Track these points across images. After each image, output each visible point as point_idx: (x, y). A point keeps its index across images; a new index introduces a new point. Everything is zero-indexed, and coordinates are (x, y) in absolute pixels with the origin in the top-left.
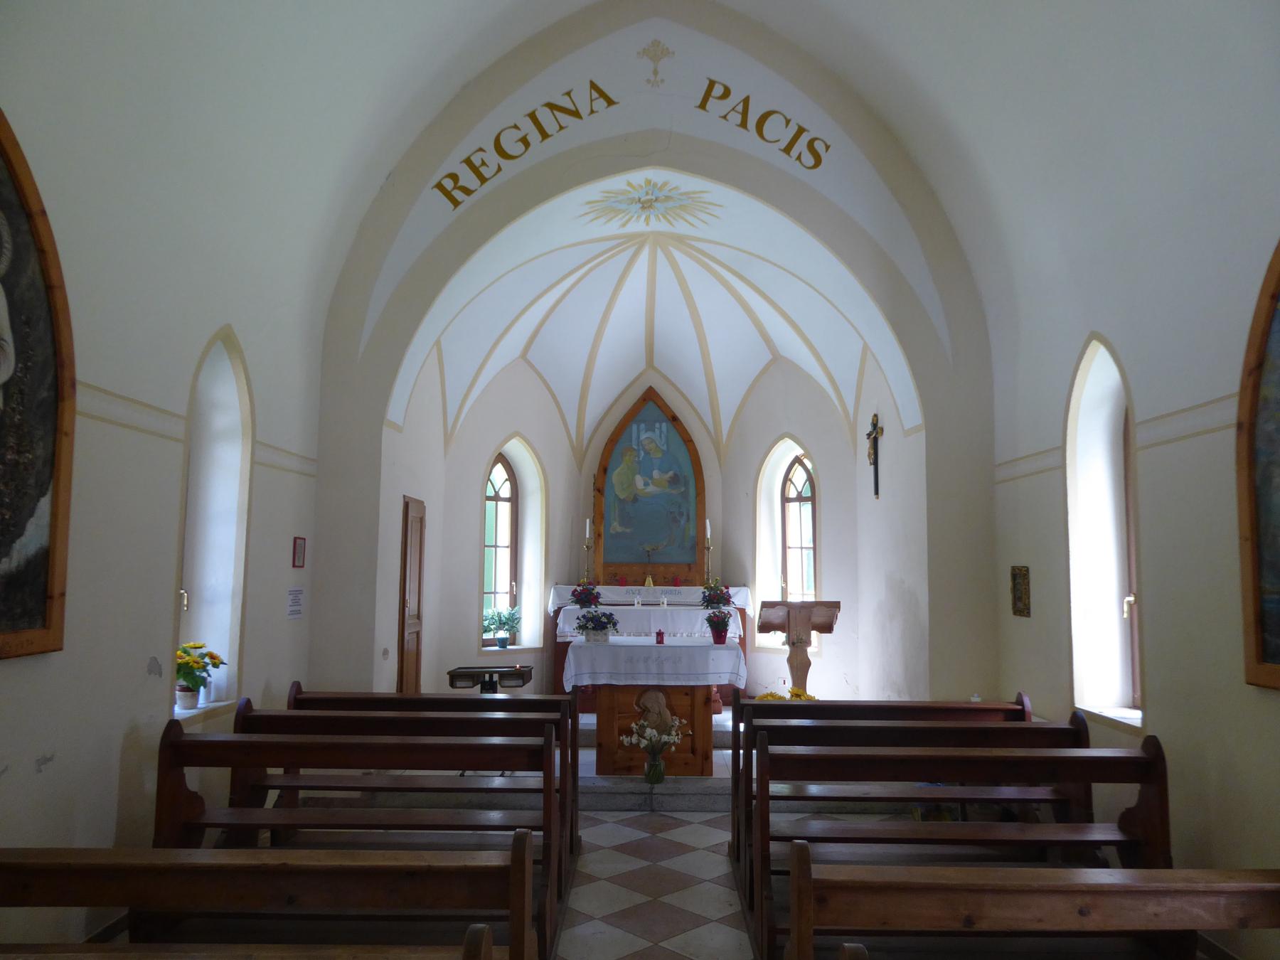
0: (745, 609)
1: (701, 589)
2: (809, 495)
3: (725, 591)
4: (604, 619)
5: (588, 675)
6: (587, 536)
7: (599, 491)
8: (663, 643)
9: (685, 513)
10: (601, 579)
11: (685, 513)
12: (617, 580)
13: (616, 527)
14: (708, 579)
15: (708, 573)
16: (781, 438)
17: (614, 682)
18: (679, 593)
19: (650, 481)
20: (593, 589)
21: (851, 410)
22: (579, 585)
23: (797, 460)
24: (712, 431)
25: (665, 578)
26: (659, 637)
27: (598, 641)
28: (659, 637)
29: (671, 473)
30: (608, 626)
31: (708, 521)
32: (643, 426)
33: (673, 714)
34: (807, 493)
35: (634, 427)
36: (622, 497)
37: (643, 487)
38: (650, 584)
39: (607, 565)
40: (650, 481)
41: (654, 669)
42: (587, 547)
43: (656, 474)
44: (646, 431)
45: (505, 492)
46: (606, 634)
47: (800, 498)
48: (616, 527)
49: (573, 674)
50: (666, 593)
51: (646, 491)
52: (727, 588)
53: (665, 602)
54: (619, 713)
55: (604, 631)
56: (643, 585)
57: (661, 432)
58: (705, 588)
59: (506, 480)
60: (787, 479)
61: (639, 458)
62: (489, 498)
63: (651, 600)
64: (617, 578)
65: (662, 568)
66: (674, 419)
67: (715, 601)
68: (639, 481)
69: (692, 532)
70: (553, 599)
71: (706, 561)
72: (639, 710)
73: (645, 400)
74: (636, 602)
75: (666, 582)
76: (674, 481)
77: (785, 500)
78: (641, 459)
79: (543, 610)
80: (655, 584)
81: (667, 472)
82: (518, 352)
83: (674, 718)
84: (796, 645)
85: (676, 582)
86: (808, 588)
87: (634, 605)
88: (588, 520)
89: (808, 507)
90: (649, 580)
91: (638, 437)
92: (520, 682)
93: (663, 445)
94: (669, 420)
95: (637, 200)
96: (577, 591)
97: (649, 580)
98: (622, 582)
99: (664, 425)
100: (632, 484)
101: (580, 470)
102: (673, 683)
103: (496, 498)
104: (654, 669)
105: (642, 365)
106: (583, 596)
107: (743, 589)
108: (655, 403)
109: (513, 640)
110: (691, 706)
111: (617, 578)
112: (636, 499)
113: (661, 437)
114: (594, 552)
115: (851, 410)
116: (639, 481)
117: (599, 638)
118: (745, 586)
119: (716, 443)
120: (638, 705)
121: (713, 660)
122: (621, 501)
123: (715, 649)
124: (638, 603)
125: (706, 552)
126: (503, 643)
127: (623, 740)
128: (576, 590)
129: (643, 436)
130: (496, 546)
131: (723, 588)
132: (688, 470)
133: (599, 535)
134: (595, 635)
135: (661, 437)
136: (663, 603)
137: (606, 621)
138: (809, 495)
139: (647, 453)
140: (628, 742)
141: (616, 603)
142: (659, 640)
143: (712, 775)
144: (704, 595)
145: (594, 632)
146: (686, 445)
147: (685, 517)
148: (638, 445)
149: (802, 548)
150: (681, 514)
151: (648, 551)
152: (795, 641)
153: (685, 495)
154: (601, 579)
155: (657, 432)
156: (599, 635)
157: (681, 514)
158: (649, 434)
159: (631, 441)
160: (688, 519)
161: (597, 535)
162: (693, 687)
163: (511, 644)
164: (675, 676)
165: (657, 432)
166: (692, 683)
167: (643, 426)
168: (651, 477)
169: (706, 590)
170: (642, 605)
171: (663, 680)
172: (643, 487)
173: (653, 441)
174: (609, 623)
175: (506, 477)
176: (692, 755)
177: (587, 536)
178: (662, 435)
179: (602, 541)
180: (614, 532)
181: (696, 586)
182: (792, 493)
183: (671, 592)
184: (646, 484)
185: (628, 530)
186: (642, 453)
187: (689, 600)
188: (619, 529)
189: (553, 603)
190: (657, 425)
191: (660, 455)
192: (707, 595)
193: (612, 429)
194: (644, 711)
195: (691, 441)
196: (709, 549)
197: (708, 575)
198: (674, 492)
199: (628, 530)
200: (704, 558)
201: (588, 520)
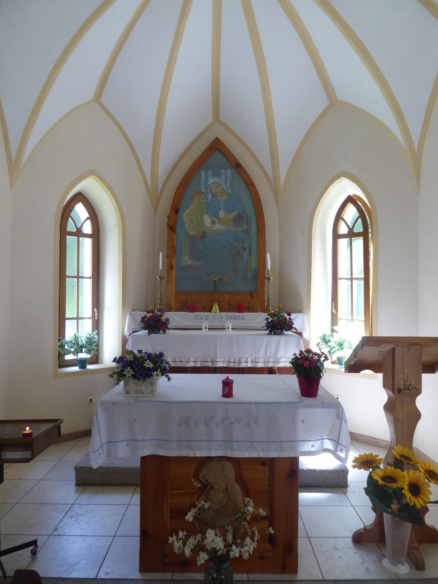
0: (302, 333)
1: (264, 315)
2: (361, 230)
3: (288, 317)
4: (148, 364)
5: (125, 443)
6: (161, 268)
7: (172, 228)
8: (232, 396)
9: (247, 248)
10: (173, 305)
11: (247, 248)
12: (187, 307)
13: (187, 260)
14: (268, 306)
15: (268, 300)
16: (337, 177)
17: (162, 453)
18: (243, 318)
19: (217, 220)
20: (161, 316)
21: (416, 139)
22: (148, 312)
23: (350, 200)
24: (271, 178)
25: (230, 305)
26: (227, 388)
27: (141, 392)
28: (227, 388)
29: (235, 214)
30: (154, 373)
31: (268, 255)
32: (210, 172)
33: (247, 493)
34: (359, 228)
35: (203, 173)
36: (192, 234)
37: (211, 226)
38: (216, 309)
39: (177, 294)
40: (217, 220)
41: (219, 433)
42: (160, 277)
43: (222, 214)
44: (213, 176)
45: (87, 228)
46: (152, 384)
47: (351, 235)
48: (187, 260)
49: (104, 440)
50: (230, 318)
51: (213, 228)
52: (289, 314)
53: (230, 327)
54: (171, 489)
55: (148, 380)
56: (210, 311)
57: (226, 177)
58: (269, 315)
59: (88, 219)
60: (339, 217)
61: (207, 200)
62: (71, 234)
63: (217, 324)
64: (187, 305)
65: (227, 296)
66: (238, 166)
67: (279, 327)
68: (207, 220)
69: (254, 264)
70: (129, 324)
71: (266, 289)
72: (199, 485)
73: (212, 149)
74: (203, 328)
75: (231, 309)
76: (238, 220)
77: (336, 236)
78: (208, 201)
79: (121, 334)
80: (221, 310)
81: (232, 212)
82: (90, 95)
83: (247, 500)
84: (403, 392)
85: (240, 309)
86: (357, 315)
87: (202, 329)
88: (161, 254)
89: (359, 243)
90: (216, 307)
91: (206, 182)
92: (27, 454)
93: (228, 189)
94: (233, 166)
95: (247, 510)
96: (147, 317)
97: (216, 307)
98: (192, 309)
99: (229, 171)
100: (201, 222)
101: (155, 210)
102: (246, 455)
103: (79, 233)
104: (219, 433)
105: (209, 119)
106: (152, 322)
107: (300, 315)
108: (221, 152)
109: (96, 360)
110: (269, 480)
111: (187, 305)
112: (203, 236)
113: (226, 182)
114: (167, 282)
115: (416, 139)
116: (207, 220)
117: (143, 388)
118: (300, 312)
119: (275, 188)
120: (198, 480)
121: (303, 421)
122: (192, 238)
123: (306, 406)
124: (205, 328)
125: (266, 281)
126: (83, 363)
127: (173, 543)
128: (145, 317)
129: (211, 181)
130: (78, 277)
131: (286, 315)
132: (250, 211)
133: (172, 267)
134: (137, 385)
135: (226, 182)
136: (228, 328)
137: (151, 366)
138: (361, 230)
139: (214, 196)
140: (179, 548)
141: (188, 327)
142: (227, 391)
143: (295, 571)
144: (268, 321)
145: (136, 381)
146: (248, 188)
147: (247, 251)
148: (206, 189)
149: (352, 279)
150: (244, 249)
151: (215, 281)
152: (402, 388)
153: (247, 232)
154: (173, 305)
155: (223, 177)
156: (144, 387)
157: (244, 249)
158: (216, 179)
159: (200, 184)
160: (250, 254)
161: (171, 267)
162: (273, 460)
163: (91, 363)
164: (249, 444)
165: (223, 177)
166: (272, 455)
167: (210, 172)
168: (217, 217)
169: (269, 317)
170: (209, 329)
171: (232, 449)
172: (211, 226)
173: (219, 185)
174: (155, 369)
175: (88, 216)
176: (269, 545)
177: (161, 268)
178: (228, 180)
179: (174, 273)
180: (184, 265)
181: (256, 311)
182: (343, 229)
183: (235, 318)
184: (213, 223)
185: (197, 263)
186: (210, 196)
187: (252, 325)
188: (189, 262)
189: (128, 328)
190: (223, 171)
191: (225, 198)
192: (269, 321)
193: (183, 175)
194: (206, 486)
195: (253, 185)
196: (269, 279)
197: (269, 303)
198: (238, 229)
199: (197, 263)
200: (264, 288)
201: (161, 254)
